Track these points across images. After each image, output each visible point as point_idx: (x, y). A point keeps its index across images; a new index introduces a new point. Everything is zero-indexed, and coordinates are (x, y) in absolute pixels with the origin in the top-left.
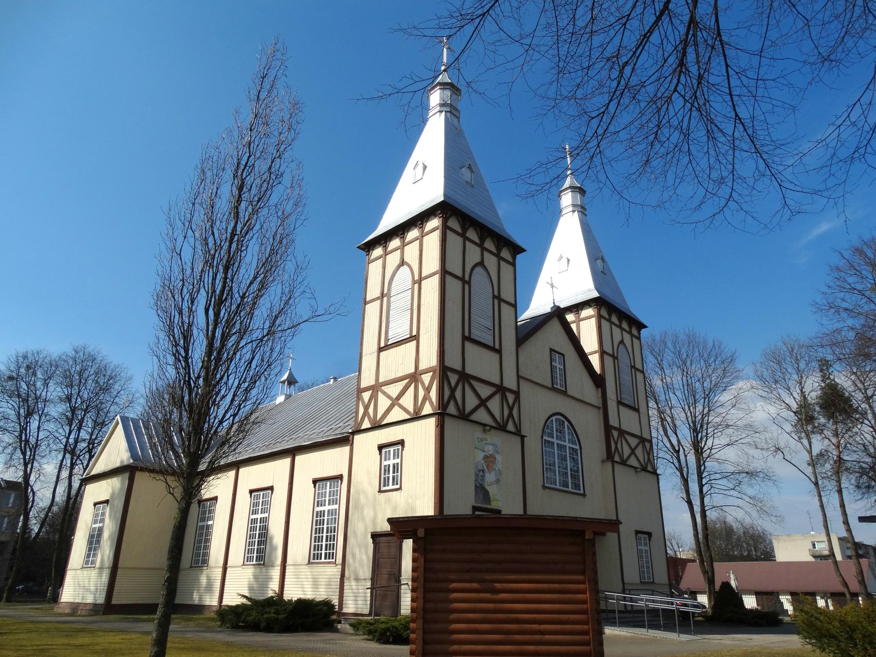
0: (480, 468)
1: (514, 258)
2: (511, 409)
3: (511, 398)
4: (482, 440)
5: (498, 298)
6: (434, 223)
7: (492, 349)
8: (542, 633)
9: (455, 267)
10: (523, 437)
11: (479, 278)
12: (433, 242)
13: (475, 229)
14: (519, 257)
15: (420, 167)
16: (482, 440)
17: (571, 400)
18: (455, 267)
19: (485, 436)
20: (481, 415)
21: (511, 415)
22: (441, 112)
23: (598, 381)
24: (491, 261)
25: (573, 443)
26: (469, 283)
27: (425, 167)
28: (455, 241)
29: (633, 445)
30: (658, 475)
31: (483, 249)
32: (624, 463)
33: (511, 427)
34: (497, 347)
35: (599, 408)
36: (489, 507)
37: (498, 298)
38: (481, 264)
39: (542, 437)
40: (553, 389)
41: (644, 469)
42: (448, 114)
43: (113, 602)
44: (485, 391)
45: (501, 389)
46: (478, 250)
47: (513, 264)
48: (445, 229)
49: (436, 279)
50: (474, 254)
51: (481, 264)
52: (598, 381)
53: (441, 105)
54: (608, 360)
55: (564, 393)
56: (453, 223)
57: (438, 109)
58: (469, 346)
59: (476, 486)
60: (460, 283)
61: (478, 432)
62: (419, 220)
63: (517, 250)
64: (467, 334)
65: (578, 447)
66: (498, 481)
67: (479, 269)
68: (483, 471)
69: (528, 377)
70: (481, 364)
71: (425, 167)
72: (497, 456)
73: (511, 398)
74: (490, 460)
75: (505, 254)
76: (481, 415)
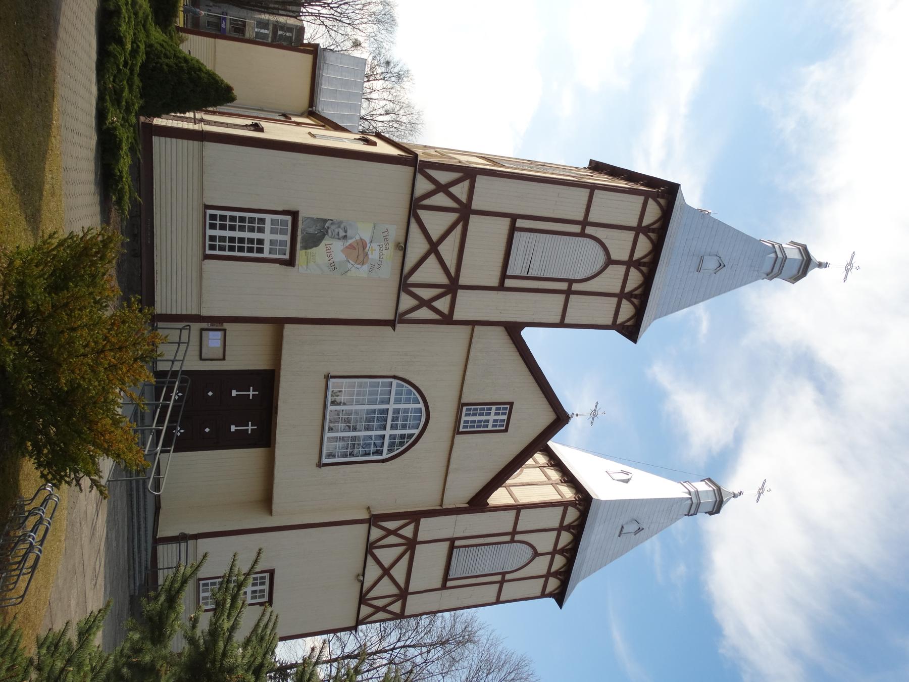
0: (349, 233)
1: (550, 595)
2: (384, 609)
3: (396, 608)
4: (386, 238)
5: (503, 579)
6: (568, 494)
7: (446, 579)
8: (138, 491)
9: (527, 520)
10: (391, 324)
11: (516, 555)
12: (548, 494)
13: (564, 566)
14: (552, 601)
15: (625, 477)
16: (386, 238)
17: (448, 444)
18: (527, 520)
19: (391, 246)
20: (373, 572)
21: (378, 609)
22: (690, 493)
23: (478, 503)
24: (540, 566)
25: (392, 445)
26: (513, 541)
27: (627, 481)
28: (553, 518)
29: (454, 190)
30: (355, 628)
31: (553, 554)
32: (370, 548)
33: (365, 610)
34: (449, 584)
35: (441, 505)
36: (299, 246)
37: (503, 579)
38: (536, 554)
39: (395, 377)
40: (461, 405)
41: (363, 599)
42: (689, 502)
43: (155, 139)
44: (399, 573)
45: (403, 594)
46: (550, 548)
47: (543, 595)
48: (565, 505)
49: (511, 501)
50: (545, 543)
51: (536, 554)
52: (478, 503)
53: (697, 492)
54: (505, 522)
55: (457, 431)
56: (572, 515)
57: (692, 490)
58: (446, 545)
59: (325, 221)
60: (510, 529)
61: (395, 233)
62: (569, 479)
63: (560, 597)
64: (457, 543)
65: (385, 456)
66: (333, 266)
67: (529, 552)
68: (345, 237)
69: (473, 340)
70: (486, 236)
71: (627, 481)
72: (365, 267)
73: (443, 304)
74: (359, 251)
75: (553, 584)
76: (373, 572)
